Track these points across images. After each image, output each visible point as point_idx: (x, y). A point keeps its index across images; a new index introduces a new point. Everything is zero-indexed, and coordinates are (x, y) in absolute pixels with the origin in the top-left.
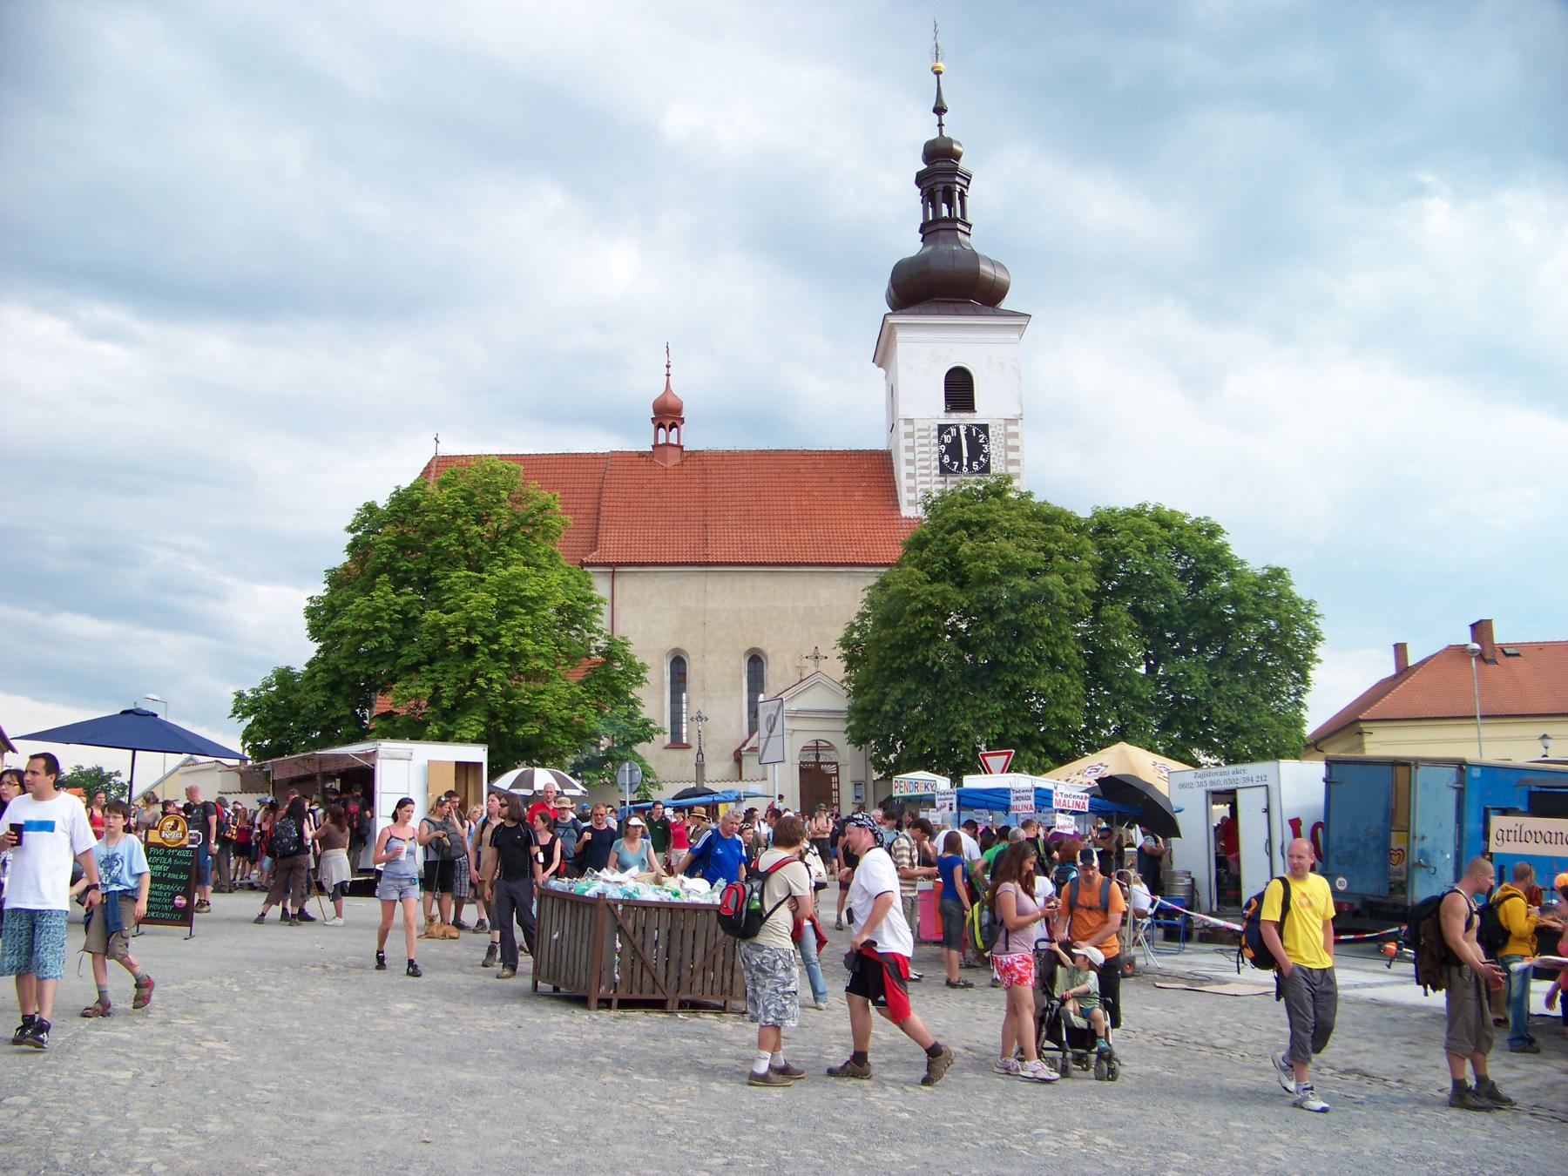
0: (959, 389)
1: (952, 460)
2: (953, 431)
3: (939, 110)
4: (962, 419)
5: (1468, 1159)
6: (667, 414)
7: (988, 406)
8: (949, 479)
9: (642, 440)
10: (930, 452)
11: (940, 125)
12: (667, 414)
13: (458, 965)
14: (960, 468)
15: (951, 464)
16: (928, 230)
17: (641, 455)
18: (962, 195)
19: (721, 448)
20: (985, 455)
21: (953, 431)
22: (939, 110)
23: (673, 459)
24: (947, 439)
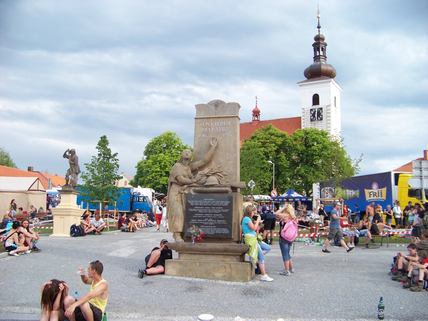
0: (316, 99)
2: (314, 110)
3: (319, 27)
4: (316, 107)
6: (256, 113)
7: (322, 103)
8: (313, 122)
10: (308, 116)
11: (319, 31)
12: (256, 113)
14: (315, 119)
15: (313, 119)
16: (316, 58)
17: (250, 123)
18: (325, 50)
19: (400, 167)
20: (322, 116)
21: (314, 110)
23: (256, 123)
24: (312, 112)
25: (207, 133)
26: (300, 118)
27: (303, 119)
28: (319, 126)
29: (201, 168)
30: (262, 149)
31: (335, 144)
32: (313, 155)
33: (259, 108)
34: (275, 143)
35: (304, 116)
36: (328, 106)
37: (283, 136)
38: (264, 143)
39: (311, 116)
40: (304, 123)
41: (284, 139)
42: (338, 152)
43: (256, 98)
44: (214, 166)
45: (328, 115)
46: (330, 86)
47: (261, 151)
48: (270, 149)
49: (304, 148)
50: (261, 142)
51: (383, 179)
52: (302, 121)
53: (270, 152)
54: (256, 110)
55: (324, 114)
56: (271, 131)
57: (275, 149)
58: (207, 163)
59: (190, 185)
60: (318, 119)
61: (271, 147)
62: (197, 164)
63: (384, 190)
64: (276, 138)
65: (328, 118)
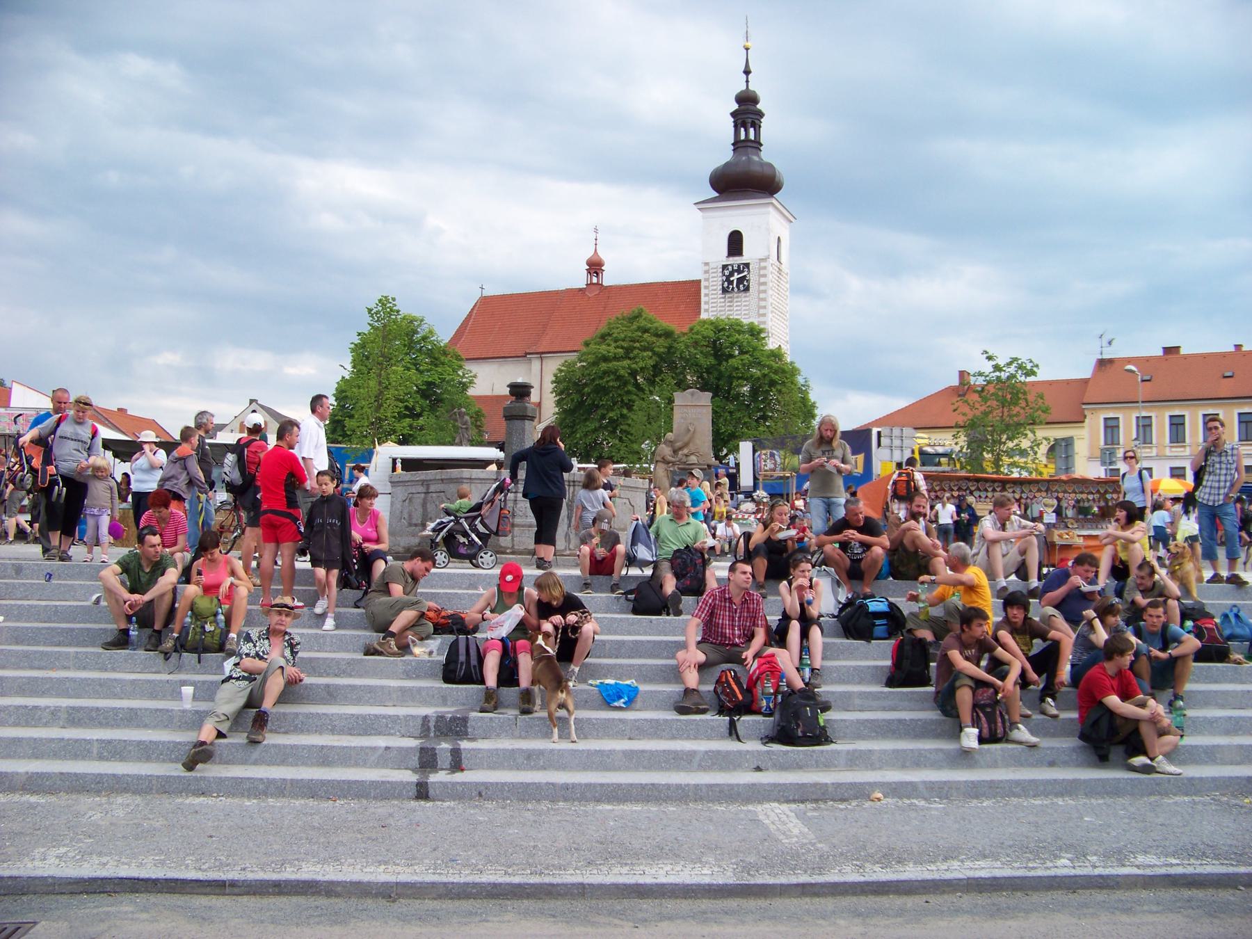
0: (735, 243)
3: (747, 72)
4: (736, 261)
6: (595, 267)
7: (750, 252)
9: (578, 278)
10: (717, 280)
11: (747, 81)
12: (595, 267)
13: (859, 676)
16: (738, 145)
17: (580, 290)
22: (747, 72)
24: (727, 273)
25: (685, 419)
26: (697, 283)
27: (706, 287)
28: (741, 310)
29: (680, 449)
30: (626, 363)
31: (777, 355)
32: (731, 378)
33: (603, 255)
34: (652, 350)
35: (707, 280)
36: (762, 260)
37: (668, 334)
38: (628, 350)
40: (706, 295)
41: (669, 341)
42: (784, 371)
43: (596, 231)
44: (692, 447)
45: (762, 280)
47: (624, 368)
48: (641, 364)
49: (712, 361)
50: (622, 347)
51: (860, 440)
52: (703, 291)
53: (642, 369)
54: (595, 259)
55: (753, 278)
56: (643, 323)
57: (651, 362)
58: (686, 445)
59: (674, 463)
60: (738, 286)
61: (643, 359)
62: (678, 444)
63: (861, 457)
64: (654, 339)
65: (762, 288)
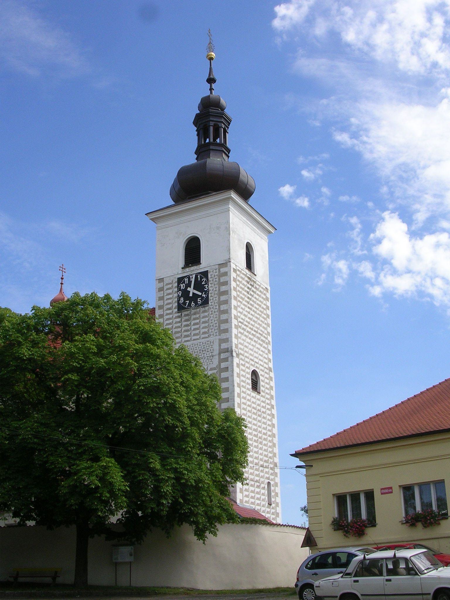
0: (193, 251)
1: (185, 300)
2: (186, 280)
3: (211, 81)
5: (172, 358)
10: (172, 296)
11: (211, 89)
15: (184, 303)
16: (202, 151)
21: (186, 280)
35: (161, 307)
39: (179, 298)
46: (228, 210)
55: (212, 287)
